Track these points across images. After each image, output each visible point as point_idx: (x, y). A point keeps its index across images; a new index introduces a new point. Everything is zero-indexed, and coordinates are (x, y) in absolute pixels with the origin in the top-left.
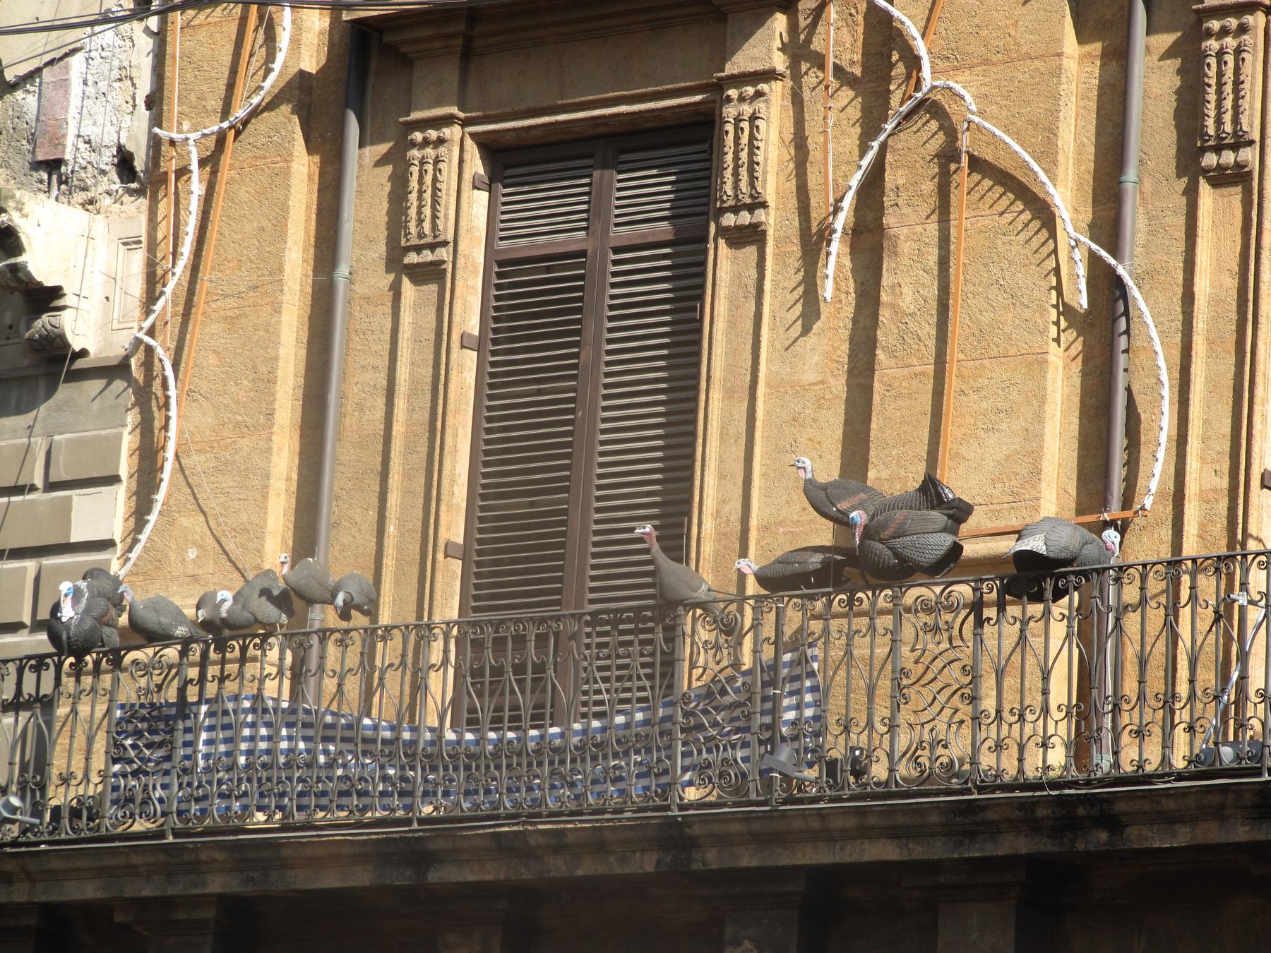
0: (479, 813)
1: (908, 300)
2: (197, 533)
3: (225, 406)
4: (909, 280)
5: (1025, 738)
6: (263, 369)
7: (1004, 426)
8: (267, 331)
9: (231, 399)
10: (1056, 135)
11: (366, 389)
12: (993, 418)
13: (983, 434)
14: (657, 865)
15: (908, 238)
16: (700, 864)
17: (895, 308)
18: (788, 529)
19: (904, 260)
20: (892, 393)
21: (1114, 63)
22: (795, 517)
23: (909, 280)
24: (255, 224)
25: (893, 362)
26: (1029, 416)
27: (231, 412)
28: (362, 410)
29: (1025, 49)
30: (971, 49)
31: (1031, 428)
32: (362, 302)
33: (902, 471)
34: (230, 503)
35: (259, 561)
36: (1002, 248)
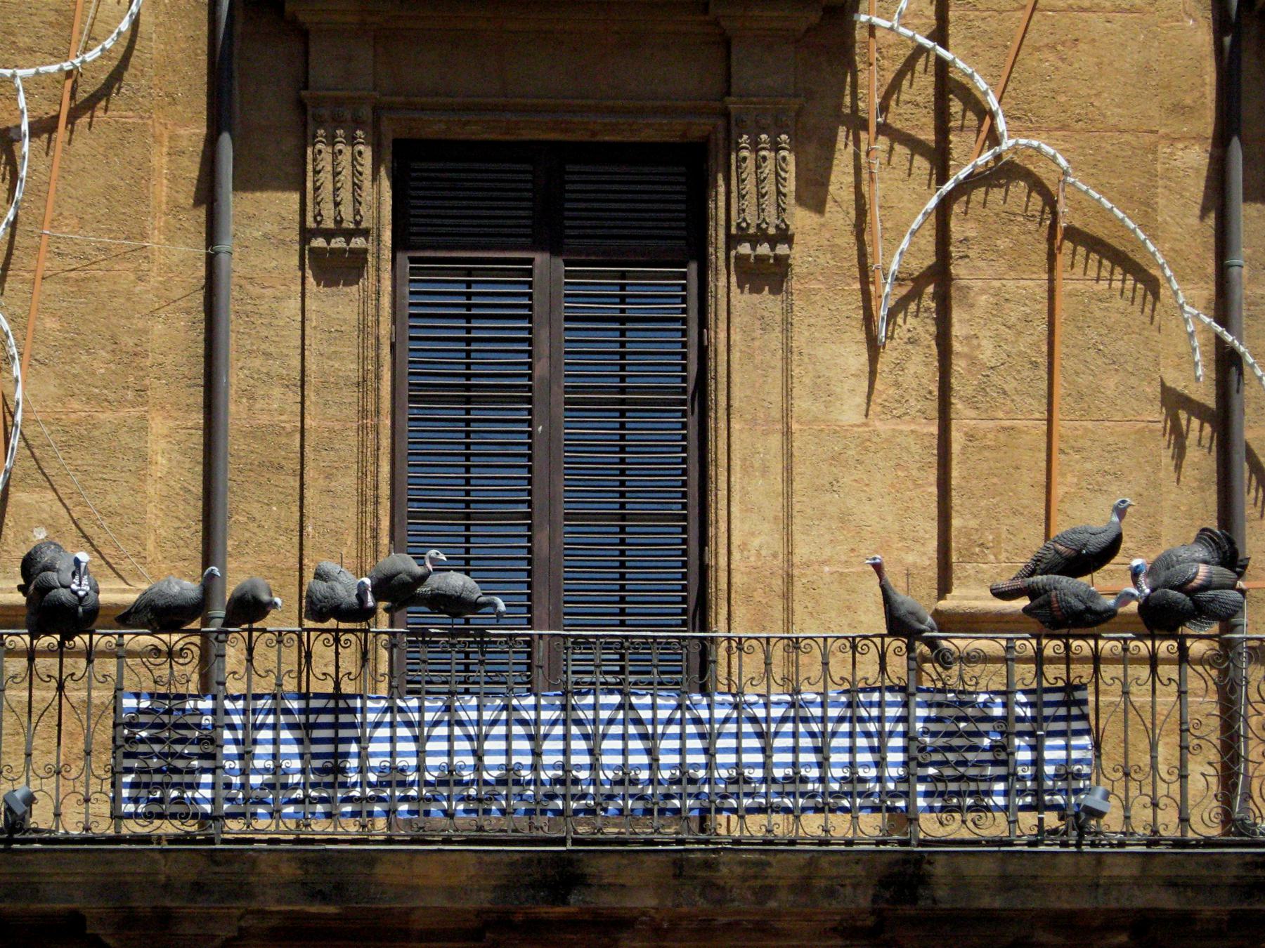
0: (600, 836)
1: (989, 353)
2: (44, 511)
3: (75, 376)
4: (989, 334)
5: (61, 797)
6: (128, 341)
7: (1114, 488)
8: (129, 299)
9: (82, 368)
10: (1155, 210)
11: (256, 376)
12: (1100, 479)
13: (1088, 495)
14: (874, 901)
15: (983, 291)
16: (929, 902)
17: (973, 361)
18: (835, 569)
19: (978, 312)
20: (975, 443)
21: (1197, 147)
22: (844, 558)
23: (989, 334)
24: (101, 181)
25: (973, 413)
26: (1143, 482)
27: (83, 383)
28: (252, 398)
29: (1112, 121)
30: (1047, 112)
31: (1145, 494)
32: (243, 282)
33: (994, 522)
34: (92, 483)
35: (140, 549)
36: (1098, 314)
